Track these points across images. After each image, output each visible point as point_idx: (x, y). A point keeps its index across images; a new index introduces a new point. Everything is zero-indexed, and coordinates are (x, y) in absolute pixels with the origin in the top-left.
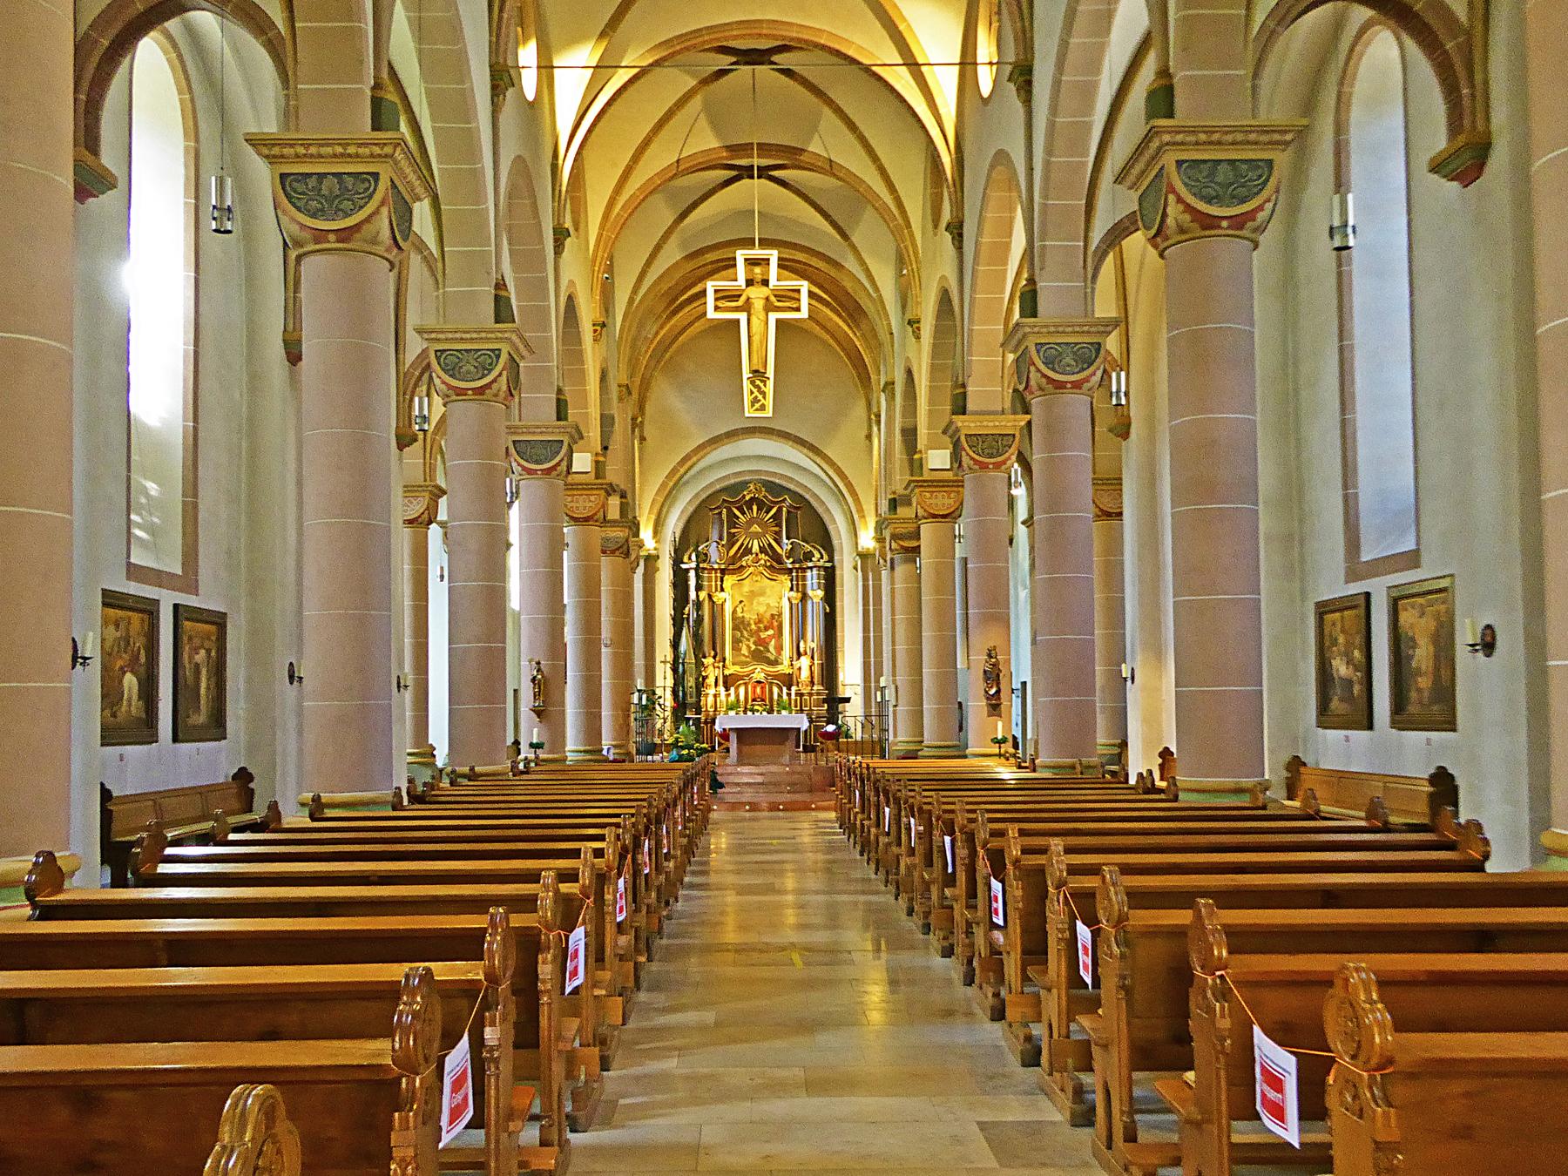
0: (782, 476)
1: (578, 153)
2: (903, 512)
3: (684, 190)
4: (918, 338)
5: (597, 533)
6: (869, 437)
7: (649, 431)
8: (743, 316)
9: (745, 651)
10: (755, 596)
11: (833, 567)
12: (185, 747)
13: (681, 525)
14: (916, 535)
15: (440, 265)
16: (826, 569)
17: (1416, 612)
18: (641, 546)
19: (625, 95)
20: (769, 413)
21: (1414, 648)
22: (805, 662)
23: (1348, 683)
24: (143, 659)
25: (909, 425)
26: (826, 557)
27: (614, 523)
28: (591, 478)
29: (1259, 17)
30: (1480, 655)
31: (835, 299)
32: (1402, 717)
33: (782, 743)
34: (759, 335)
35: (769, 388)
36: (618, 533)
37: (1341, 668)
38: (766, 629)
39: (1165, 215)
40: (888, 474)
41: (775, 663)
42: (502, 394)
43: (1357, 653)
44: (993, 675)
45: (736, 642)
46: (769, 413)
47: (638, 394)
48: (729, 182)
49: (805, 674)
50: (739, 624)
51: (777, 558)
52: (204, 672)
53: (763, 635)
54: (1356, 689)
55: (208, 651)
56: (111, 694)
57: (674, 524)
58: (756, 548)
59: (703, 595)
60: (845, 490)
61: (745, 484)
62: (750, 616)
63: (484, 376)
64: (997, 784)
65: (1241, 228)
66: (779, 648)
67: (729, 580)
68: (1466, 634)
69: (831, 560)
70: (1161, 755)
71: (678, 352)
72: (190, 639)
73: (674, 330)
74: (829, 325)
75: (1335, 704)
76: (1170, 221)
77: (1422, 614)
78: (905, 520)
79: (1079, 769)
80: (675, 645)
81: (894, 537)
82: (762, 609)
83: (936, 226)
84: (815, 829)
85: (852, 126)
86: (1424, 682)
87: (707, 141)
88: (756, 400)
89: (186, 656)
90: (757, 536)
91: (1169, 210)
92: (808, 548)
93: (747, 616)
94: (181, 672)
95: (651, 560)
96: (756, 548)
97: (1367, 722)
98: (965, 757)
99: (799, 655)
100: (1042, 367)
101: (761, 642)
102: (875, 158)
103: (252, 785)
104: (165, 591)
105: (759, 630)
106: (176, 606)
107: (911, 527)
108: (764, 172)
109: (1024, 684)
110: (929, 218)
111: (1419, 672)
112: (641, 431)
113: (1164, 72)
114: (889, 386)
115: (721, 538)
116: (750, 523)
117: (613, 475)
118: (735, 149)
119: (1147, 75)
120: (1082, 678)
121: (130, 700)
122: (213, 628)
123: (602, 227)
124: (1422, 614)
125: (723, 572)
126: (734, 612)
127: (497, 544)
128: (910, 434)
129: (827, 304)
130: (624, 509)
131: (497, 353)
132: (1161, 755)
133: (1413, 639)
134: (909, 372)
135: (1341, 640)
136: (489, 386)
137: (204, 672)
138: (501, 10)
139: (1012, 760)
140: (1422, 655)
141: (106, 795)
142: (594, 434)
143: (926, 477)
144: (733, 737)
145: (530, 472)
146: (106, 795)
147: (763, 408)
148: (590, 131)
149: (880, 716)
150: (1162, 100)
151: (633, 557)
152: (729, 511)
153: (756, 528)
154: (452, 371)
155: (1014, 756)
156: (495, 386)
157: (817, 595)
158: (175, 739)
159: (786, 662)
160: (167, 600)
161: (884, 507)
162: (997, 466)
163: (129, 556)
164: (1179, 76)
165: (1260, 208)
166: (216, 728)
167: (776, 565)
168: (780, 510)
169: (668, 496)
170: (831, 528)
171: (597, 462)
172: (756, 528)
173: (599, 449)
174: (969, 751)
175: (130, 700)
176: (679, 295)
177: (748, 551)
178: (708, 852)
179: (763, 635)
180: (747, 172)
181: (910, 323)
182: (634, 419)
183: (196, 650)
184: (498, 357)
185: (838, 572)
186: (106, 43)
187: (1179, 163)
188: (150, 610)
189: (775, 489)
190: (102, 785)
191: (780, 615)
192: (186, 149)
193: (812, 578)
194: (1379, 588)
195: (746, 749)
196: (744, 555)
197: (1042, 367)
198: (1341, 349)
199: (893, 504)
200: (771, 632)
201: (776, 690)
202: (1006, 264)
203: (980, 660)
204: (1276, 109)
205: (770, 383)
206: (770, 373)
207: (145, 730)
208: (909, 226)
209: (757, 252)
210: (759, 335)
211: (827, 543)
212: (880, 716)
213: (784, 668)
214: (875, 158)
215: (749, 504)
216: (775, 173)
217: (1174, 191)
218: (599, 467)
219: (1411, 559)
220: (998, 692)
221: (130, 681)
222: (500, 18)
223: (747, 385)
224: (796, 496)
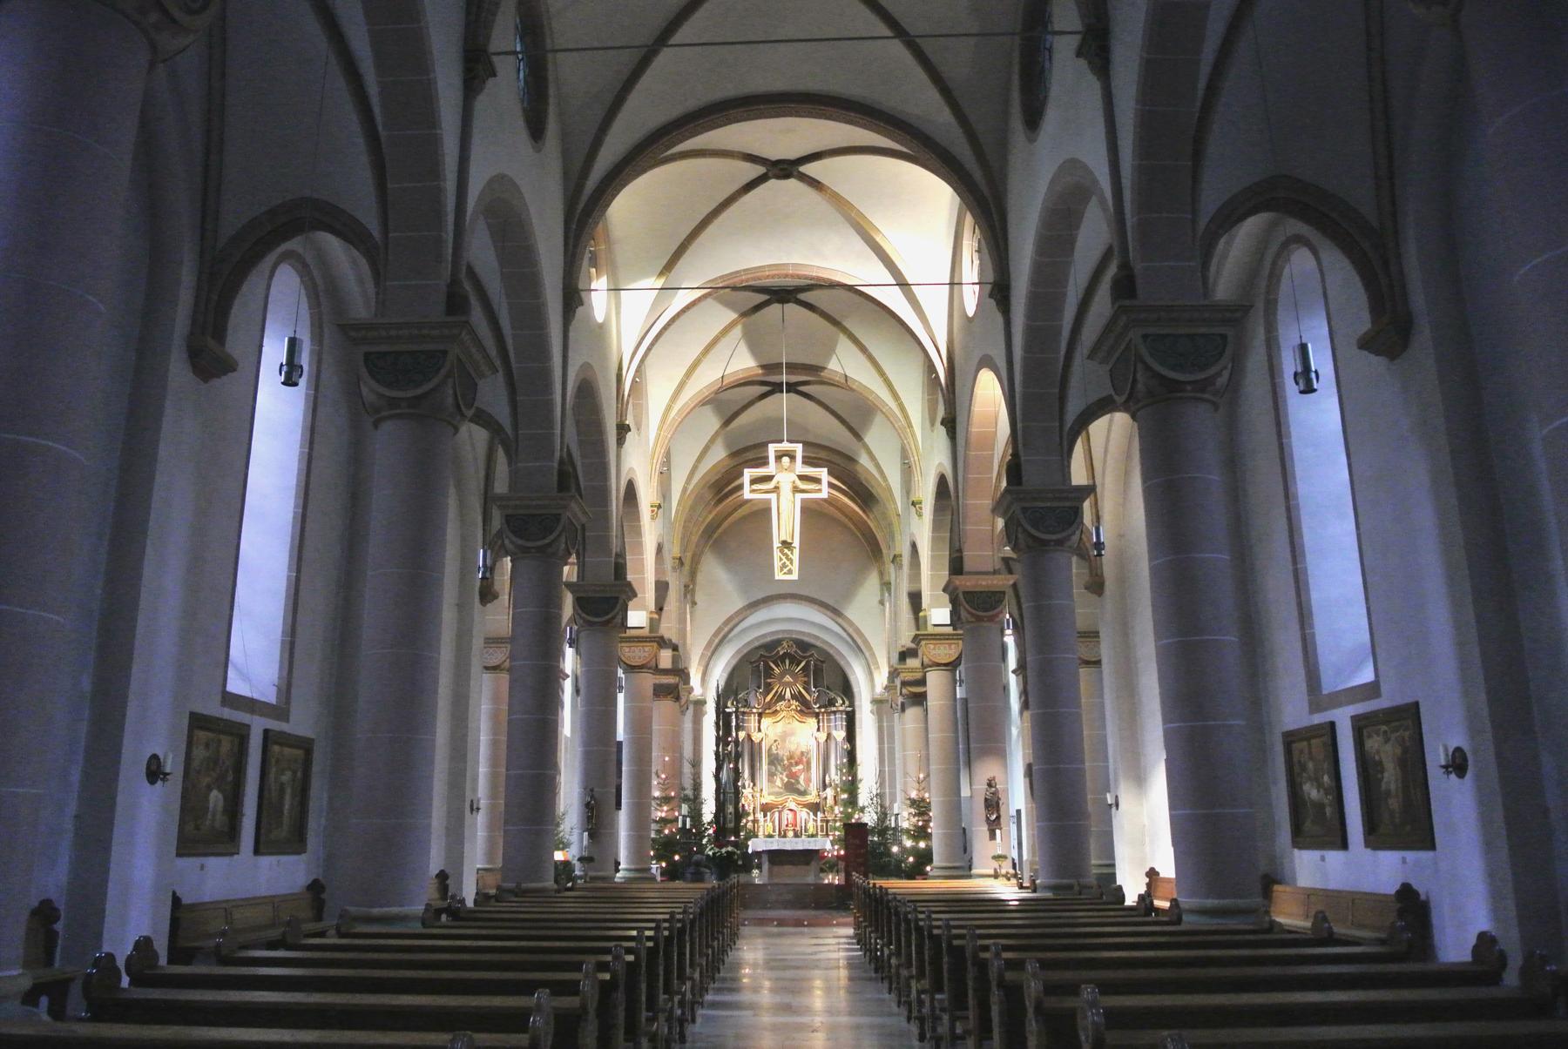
0: (809, 635)
1: (639, 367)
2: (912, 663)
3: (727, 403)
4: (920, 515)
5: (648, 681)
6: (882, 603)
7: (699, 597)
8: (773, 496)
9: (779, 783)
10: (788, 732)
11: (853, 712)
12: (266, 861)
13: (725, 676)
14: (922, 682)
16: (847, 713)
17: (1380, 739)
18: (691, 690)
19: (678, 322)
20: (795, 576)
21: (1382, 772)
22: (830, 792)
23: (1320, 807)
24: (230, 778)
25: (914, 588)
27: (666, 672)
28: (646, 632)
29: (1203, 223)
30: (1453, 776)
32: (1376, 836)
33: (808, 863)
34: (786, 522)
35: (796, 556)
36: (671, 680)
37: (1312, 792)
39: (1135, 381)
40: (895, 631)
43: (1326, 778)
44: (993, 804)
46: (795, 576)
47: (689, 566)
48: (763, 396)
49: (830, 801)
52: (289, 791)
53: (794, 769)
54: (1328, 810)
55: (295, 773)
56: (191, 807)
57: (719, 672)
58: (788, 695)
59: (742, 735)
60: (859, 647)
61: (778, 642)
62: (783, 753)
64: (997, 905)
65: (1203, 390)
66: (808, 780)
67: (766, 721)
68: (1436, 756)
69: (852, 704)
71: (725, 532)
72: (278, 761)
73: (723, 522)
75: (1308, 825)
76: (1140, 386)
77: (1387, 741)
78: (912, 670)
79: (1076, 888)
81: (904, 684)
82: (793, 748)
83: (932, 424)
84: (834, 944)
85: (863, 349)
86: (1394, 804)
87: (743, 362)
88: (784, 566)
89: (272, 776)
90: (788, 684)
91: (1139, 376)
93: (781, 753)
94: (266, 794)
95: (700, 704)
96: (788, 695)
97: (1344, 845)
98: (970, 877)
99: (825, 787)
100: (1029, 528)
101: (793, 776)
102: (882, 374)
103: (324, 896)
104: (256, 717)
106: (266, 732)
107: (918, 676)
108: (792, 388)
109: (1019, 812)
111: (1388, 793)
112: (693, 596)
113: (1125, 266)
114: (896, 559)
116: (783, 675)
117: (668, 629)
118: (770, 368)
119: (1112, 270)
120: (1070, 815)
121: (214, 815)
122: (299, 753)
123: (660, 428)
124: (1387, 741)
125: (760, 715)
127: (549, 678)
128: (915, 599)
130: (675, 660)
133: (1380, 763)
134: (914, 546)
135: (1310, 765)
136: (549, 545)
137: (289, 791)
139: (1014, 881)
140: (1390, 777)
141: (176, 901)
142: (648, 594)
143: (930, 630)
144: (765, 858)
146: (176, 901)
147: (790, 572)
148: (649, 349)
150: (1125, 287)
151: (683, 700)
153: (788, 678)
155: (1015, 876)
157: (840, 735)
158: (257, 852)
159: (814, 792)
160: (258, 725)
161: (896, 657)
162: (991, 619)
163: (225, 685)
164: (1138, 267)
165: (1219, 374)
166: (295, 842)
167: (806, 709)
169: (714, 649)
170: (852, 678)
171: (651, 620)
172: (788, 678)
173: (652, 607)
174: (974, 871)
175: (214, 815)
176: (723, 486)
177: (781, 697)
178: (737, 966)
179: (794, 769)
180: (776, 388)
181: (913, 504)
182: (686, 586)
183: (282, 772)
185: (857, 716)
186: (655, 727)
187: (1145, 337)
188: (240, 734)
189: (803, 646)
190: (174, 893)
194: (1343, 718)
195: (776, 869)
197: (1029, 528)
198: (1288, 509)
199: (903, 656)
201: (634, 933)
203: (981, 786)
204: (1224, 288)
205: (796, 552)
206: (796, 543)
207: (224, 840)
208: (910, 425)
209: (785, 446)
210: (786, 522)
211: (847, 690)
214: (882, 374)
215: (783, 658)
218: (654, 624)
219: (1372, 690)
220: (998, 818)
221: (216, 798)
223: (777, 554)
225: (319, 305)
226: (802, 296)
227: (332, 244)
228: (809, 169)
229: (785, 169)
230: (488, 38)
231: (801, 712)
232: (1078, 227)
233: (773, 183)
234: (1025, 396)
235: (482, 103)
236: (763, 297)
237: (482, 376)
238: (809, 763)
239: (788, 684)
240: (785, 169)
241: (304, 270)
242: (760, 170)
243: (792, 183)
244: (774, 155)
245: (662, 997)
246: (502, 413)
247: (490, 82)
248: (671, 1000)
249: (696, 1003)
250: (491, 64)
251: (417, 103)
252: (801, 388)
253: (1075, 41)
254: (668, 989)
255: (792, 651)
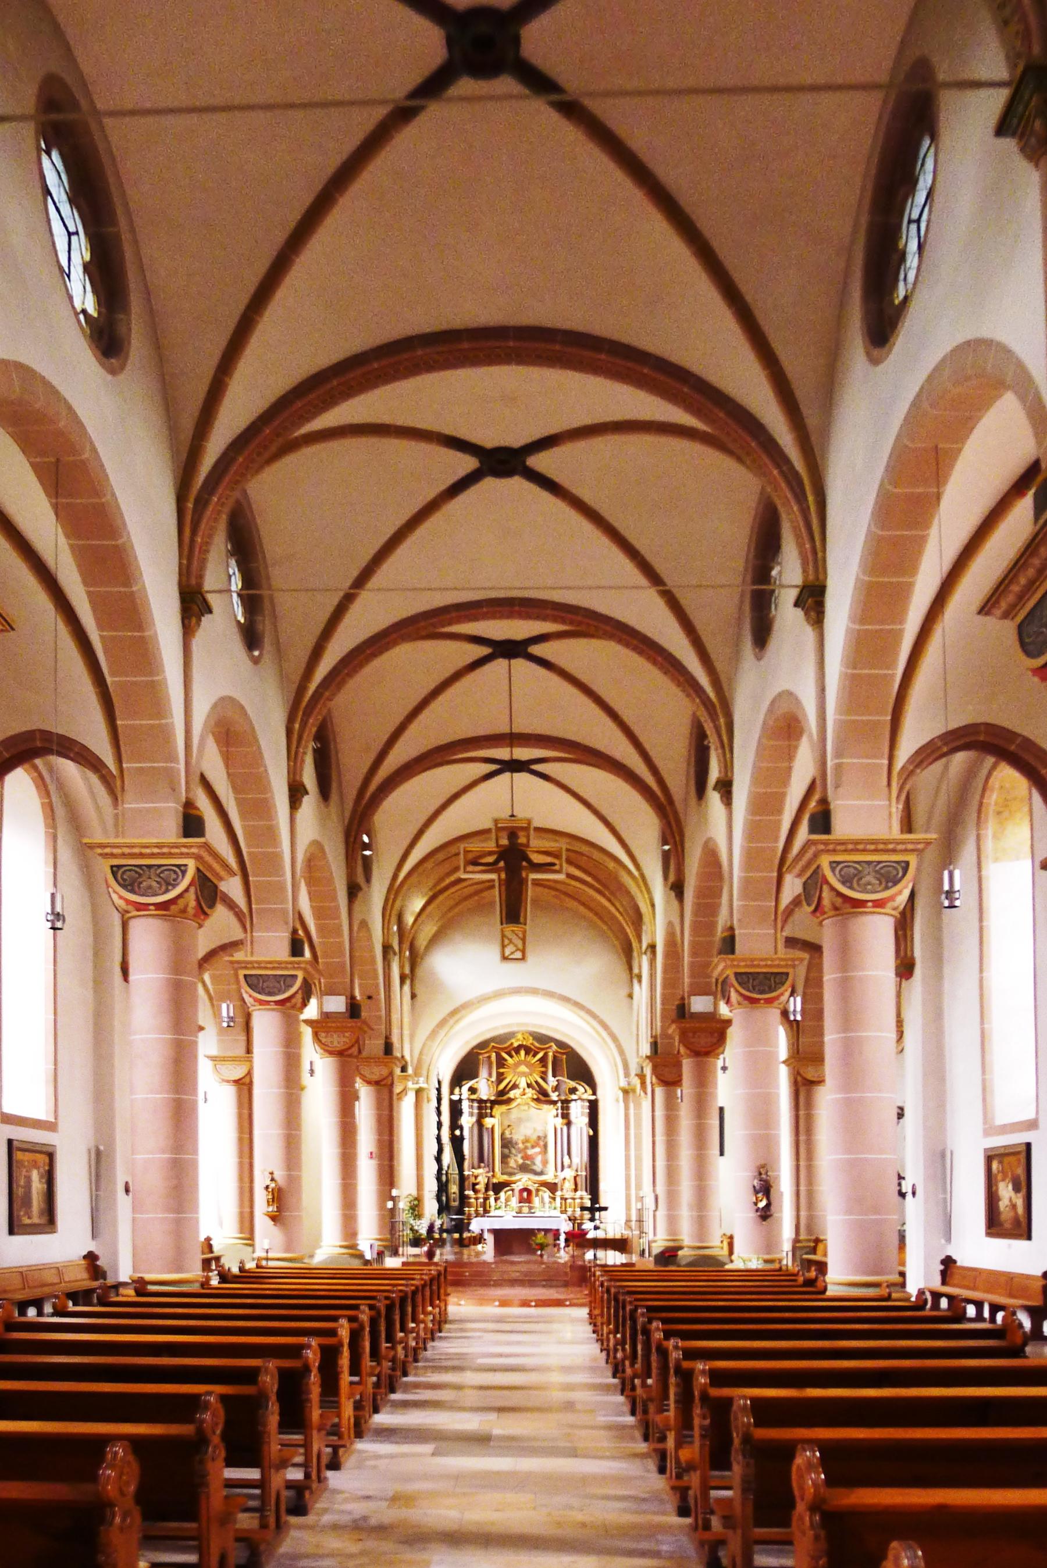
10: (532, 1121)
15: (118, 783)
16: (590, 1101)
26: (590, 1091)
31: (594, 878)
38: (533, 1147)
41: (541, 1173)
42: (191, 911)
45: (504, 1158)
50: (507, 1144)
51: (545, 1094)
53: (530, 1152)
63: (167, 891)
66: (545, 1163)
70: (943, 1262)
74: (592, 905)
80: (438, 1159)
90: (524, 1074)
92: (572, 1084)
105: (526, 1148)
110: (692, 782)
115: (490, 1075)
126: (503, 1134)
129: (591, 886)
131: (183, 869)
132: (943, 1262)
138: (194, 532)
145: (262, 1003)
149: (640, 1221)
152: (498, 1056)
154: (130, 886)
156: (181, 902)
167: (543, 1097)
168: (546, 1055)
172: (523, 1068)
184: (184, 873)
189: (543, 1039)
191: (545, 1137)
192: (43, 804)
193: (579, 1112)
196: (512, 1088)
200: (537, 1150)
202: (902, 621)
212: (640, 1221)
213: (549, 1177)
215: (517, 1050)
216: (535, 767)
217: (827, 882)
220: (768, 1205)
222: (192, 541)
224: (561, 1044)
225: (48, 794)
226: (535, 650)
227: (69, 768)
228: (538, 462)
229: (502, 462)
230: (201, 577)
231: (537, 1100)
232: (945, 482)
233: (489, 484)
234: (841, 725)
235: (196, 643)
236: (485, 651)
237: (221, 879)
238: (545, 1146)
239: (524, 1074)
240: (502, 462)
241: (41, 784)
242: (468, 463)
243: (517, 484)
244: (489, 438)
245: (385, 1345)
246: (241, 901)
247: (206, 619)
248: (393, 1348)
249: (415, 1354)
250: (205, 601)
251: (142, 655)
252: (535, 767)
253: (995, 101)
254: (390, 1338)
255: (529, 1042)
